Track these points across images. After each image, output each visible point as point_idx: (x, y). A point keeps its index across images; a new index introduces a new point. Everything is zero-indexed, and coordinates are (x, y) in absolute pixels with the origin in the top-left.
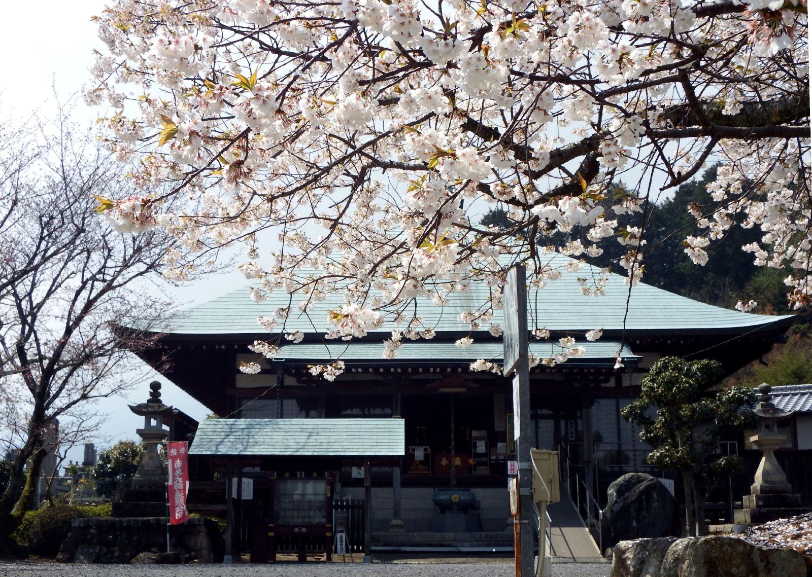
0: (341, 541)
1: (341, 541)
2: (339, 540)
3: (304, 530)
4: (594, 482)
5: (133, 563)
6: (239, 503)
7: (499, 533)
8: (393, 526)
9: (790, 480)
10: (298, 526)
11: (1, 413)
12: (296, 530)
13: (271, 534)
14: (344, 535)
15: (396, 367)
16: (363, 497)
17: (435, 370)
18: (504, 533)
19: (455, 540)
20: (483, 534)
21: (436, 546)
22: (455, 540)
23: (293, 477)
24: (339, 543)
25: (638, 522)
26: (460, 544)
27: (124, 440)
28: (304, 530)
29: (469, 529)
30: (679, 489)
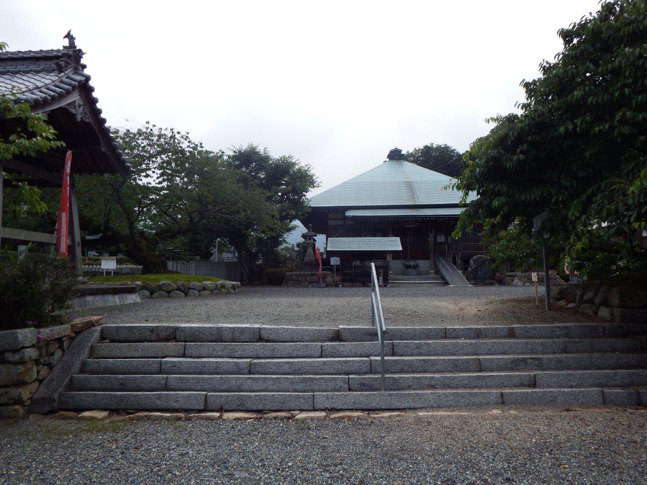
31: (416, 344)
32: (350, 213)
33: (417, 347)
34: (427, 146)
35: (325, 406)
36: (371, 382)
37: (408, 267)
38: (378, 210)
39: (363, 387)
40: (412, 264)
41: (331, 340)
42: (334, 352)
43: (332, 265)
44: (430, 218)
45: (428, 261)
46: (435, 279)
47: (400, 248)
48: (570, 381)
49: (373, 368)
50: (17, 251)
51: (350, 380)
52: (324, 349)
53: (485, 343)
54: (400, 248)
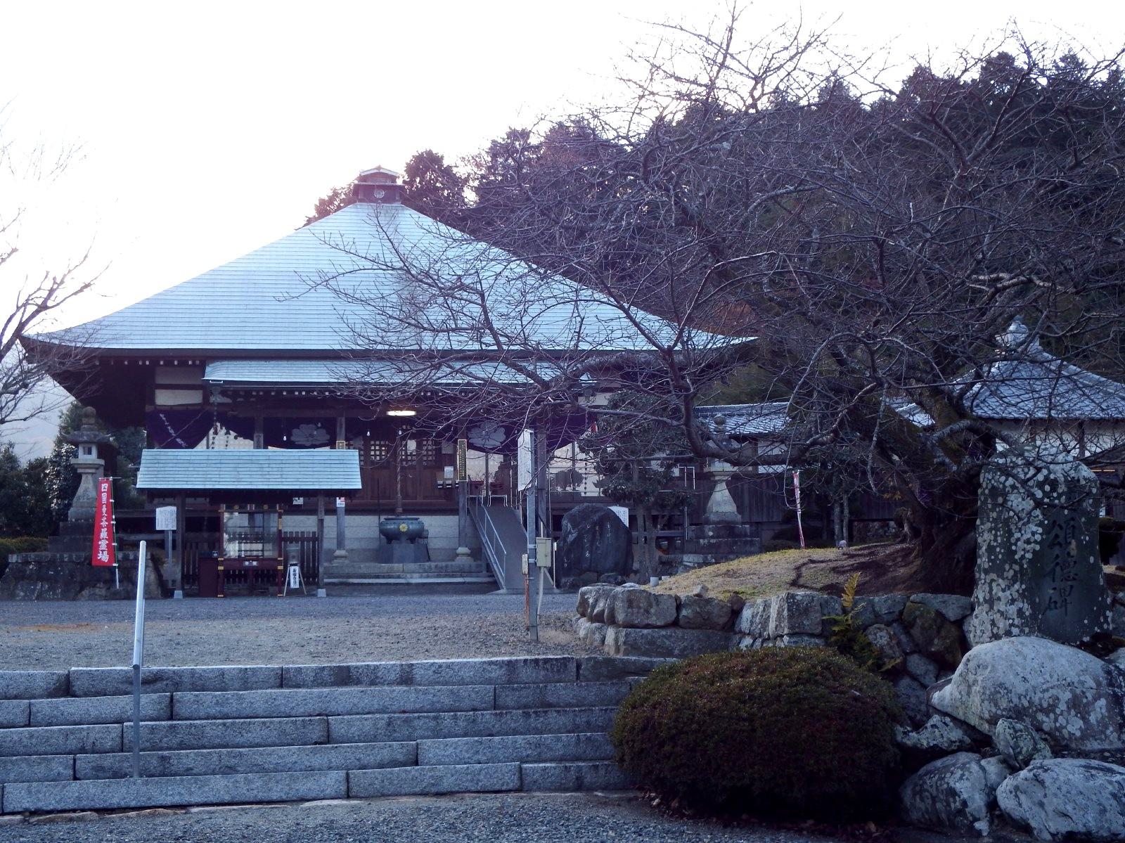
0: (295, 575)
1: (295, 575)
2: (292, 573)
3: (255, 563)
4: (547, 509)
5: (79, 600)
6: (212, 554)
7: (450, 563)
8: (337, 557)
9: (740, 509)
10: (248, 560)
11: (1123, 399)
12: (247, 563)
13: (221, 568)
14: (297, 568)
15: (144, 359)
16: (315, 529)
17: (194, 362)
18: (453, 563)
19: (403, 571)
20: (433, 564)
21: (384, 577)
22: (403, 571)
23: (272, 510)
24: (292, 577)
25: (591, 553)
26: (408, 575)
27: (33, 460)
28: (255, 563)
29: (416, 560)
30: (632, 518)
31: (216, 696)
32: (218, 373)
33: (217, 703)
34: (1006, 59)
35: (24, 806)
36: (117, 765)
37: (390, 537)
38: (254, 363)
39: (99, 772)
40: (404, 527)
41: (51, 695)
42: (55, 716)
43: (162, 532)
44: (291, 391)
45: (456, 518)
46: (469, 573)
47: (360, 487)
48: (477, 752)
49: (126, 741)
50: (326, 514)
51: (78, 762)
52: (34, 709)
53: (347, 693)
54: (360, 487)
